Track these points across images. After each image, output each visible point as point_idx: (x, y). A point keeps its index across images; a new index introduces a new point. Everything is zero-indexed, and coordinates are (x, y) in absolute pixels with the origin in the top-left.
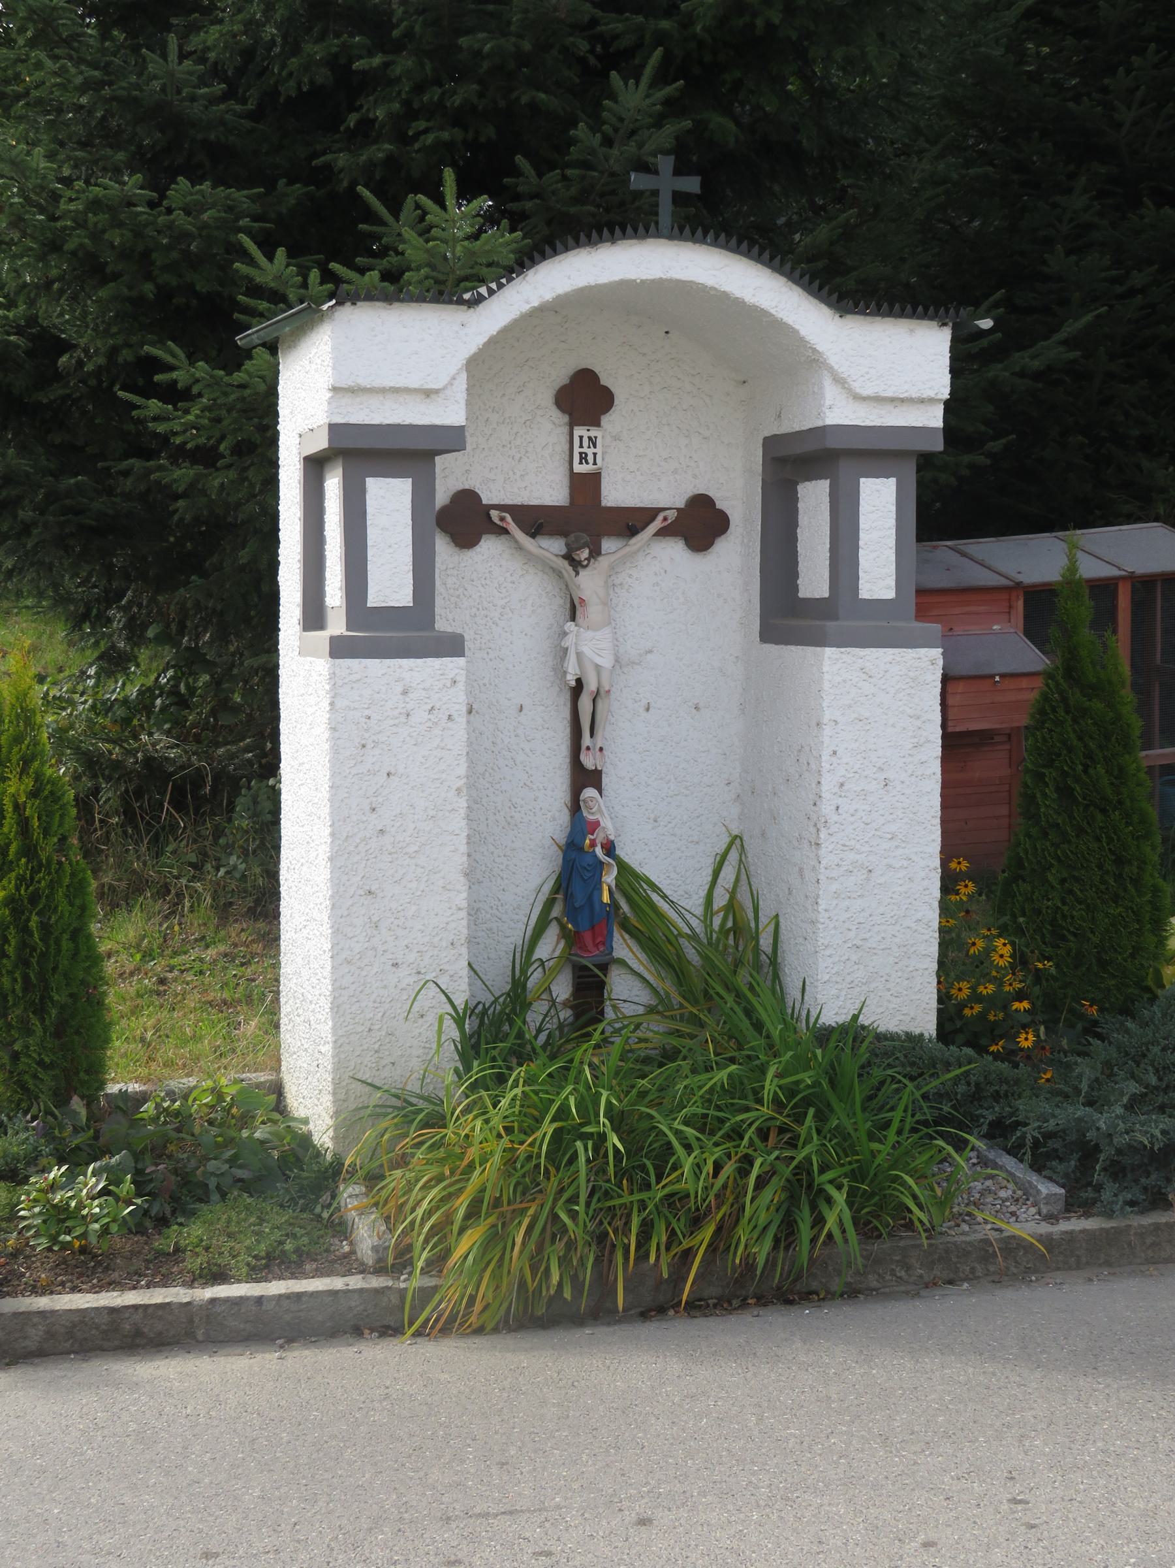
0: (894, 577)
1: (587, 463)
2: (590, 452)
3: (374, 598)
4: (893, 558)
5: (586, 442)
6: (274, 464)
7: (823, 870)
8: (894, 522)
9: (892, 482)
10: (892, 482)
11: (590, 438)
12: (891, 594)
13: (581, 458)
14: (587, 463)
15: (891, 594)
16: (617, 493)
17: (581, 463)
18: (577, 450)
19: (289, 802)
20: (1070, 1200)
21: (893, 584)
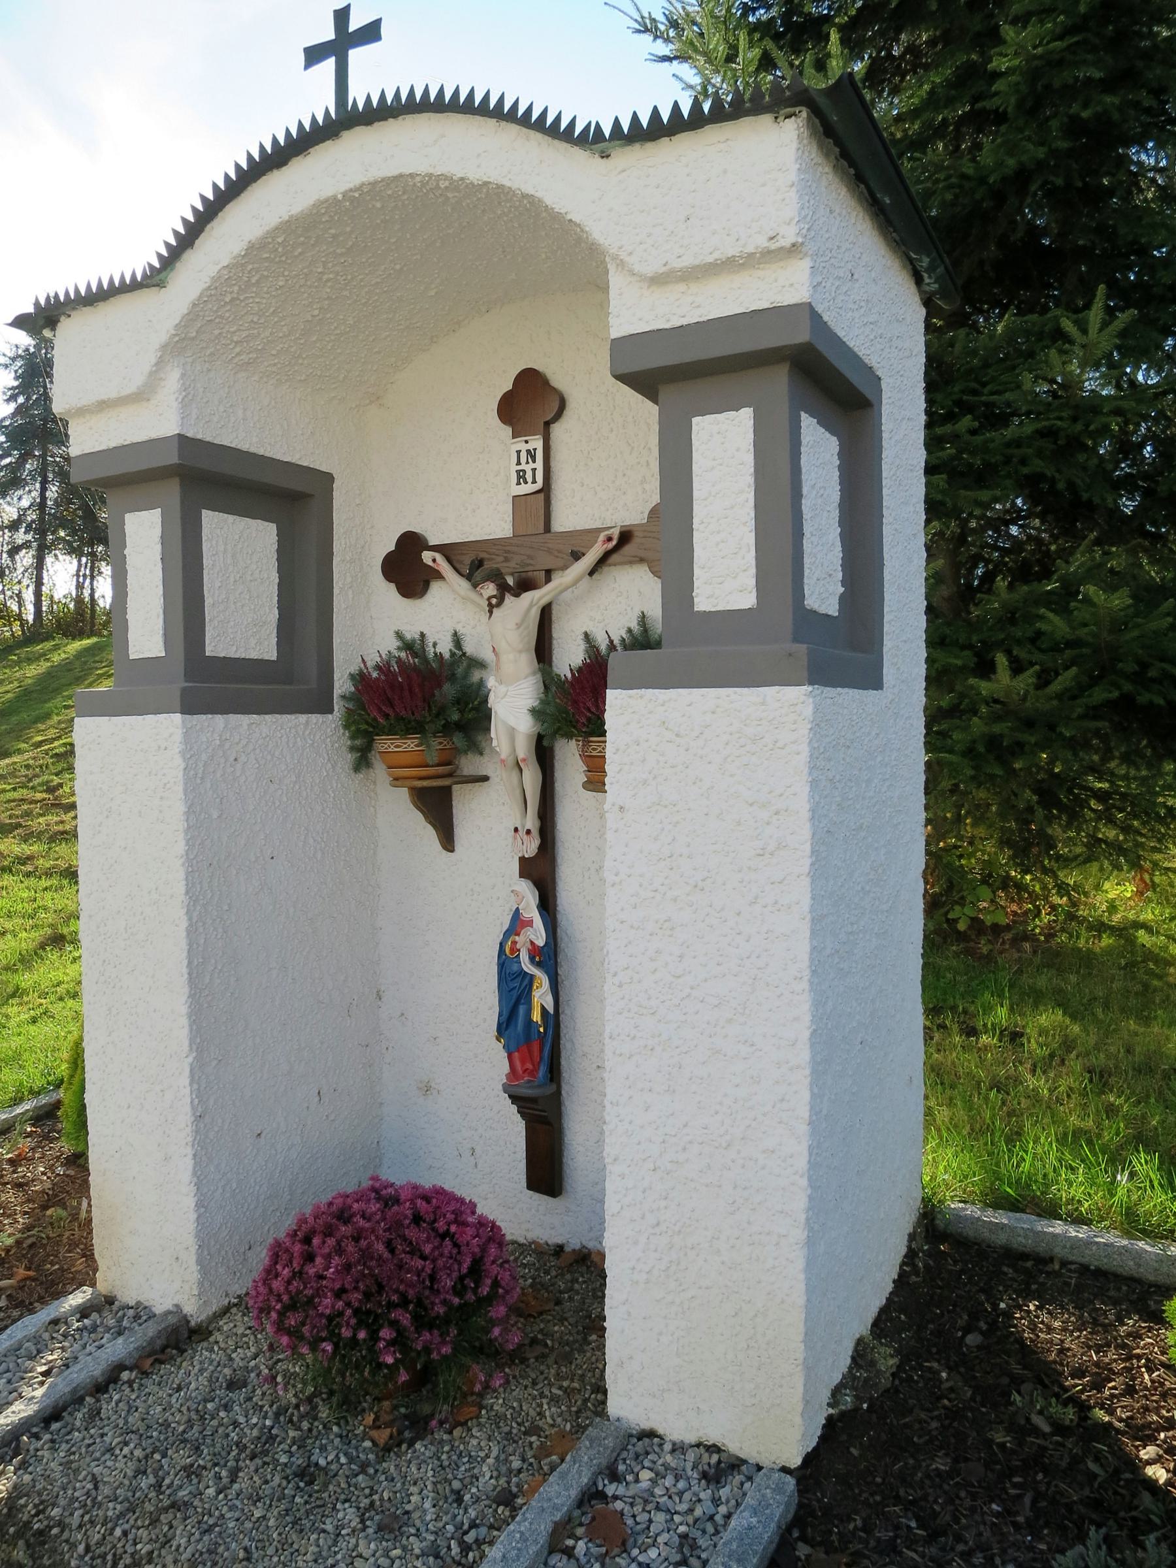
0: (753, 571)
1: (526, 482)
2: (528, 468)
3: (216, 645)
4: (752, 541)
5: (523, 455)
6: (936, 641)
7: (607, 1041)
8: (751, 480)
9: (745, 416)
10: (745, 416)
11: (528, 451)
12: (747, 600)
13: (519, 477)
14: (526, 482)
15: (747, 600)
16: (570, 516)
17: (519, 483)
18: (539, 464)
19: (612, 1377)
20: (600, 1397)
21: (752, 582)
